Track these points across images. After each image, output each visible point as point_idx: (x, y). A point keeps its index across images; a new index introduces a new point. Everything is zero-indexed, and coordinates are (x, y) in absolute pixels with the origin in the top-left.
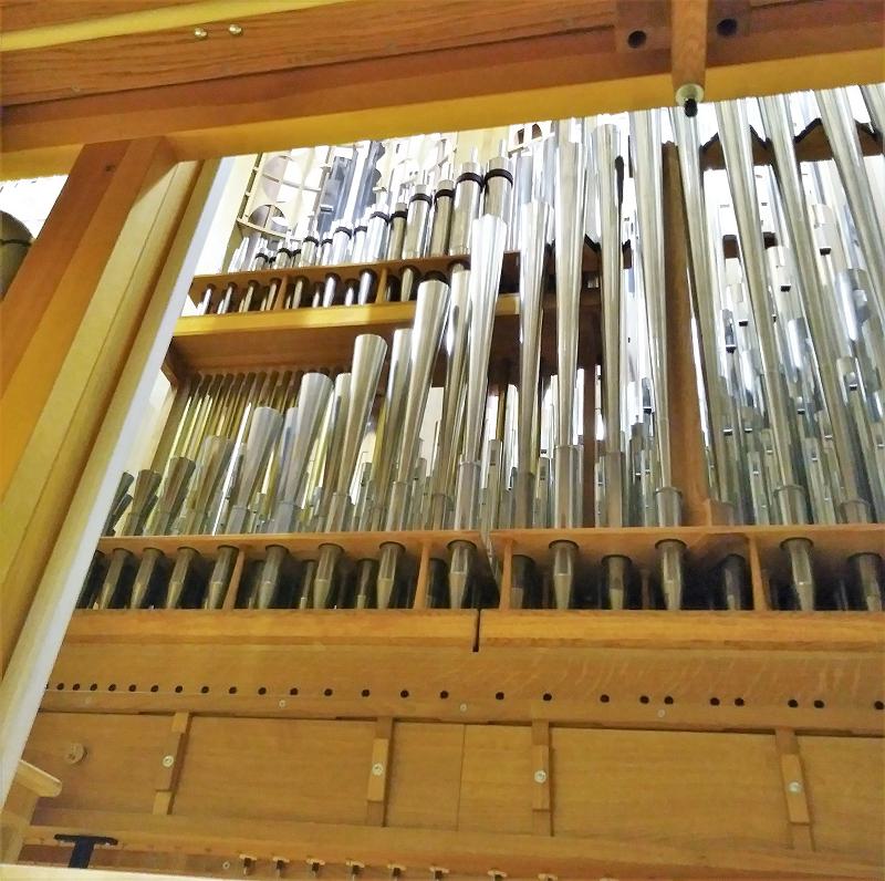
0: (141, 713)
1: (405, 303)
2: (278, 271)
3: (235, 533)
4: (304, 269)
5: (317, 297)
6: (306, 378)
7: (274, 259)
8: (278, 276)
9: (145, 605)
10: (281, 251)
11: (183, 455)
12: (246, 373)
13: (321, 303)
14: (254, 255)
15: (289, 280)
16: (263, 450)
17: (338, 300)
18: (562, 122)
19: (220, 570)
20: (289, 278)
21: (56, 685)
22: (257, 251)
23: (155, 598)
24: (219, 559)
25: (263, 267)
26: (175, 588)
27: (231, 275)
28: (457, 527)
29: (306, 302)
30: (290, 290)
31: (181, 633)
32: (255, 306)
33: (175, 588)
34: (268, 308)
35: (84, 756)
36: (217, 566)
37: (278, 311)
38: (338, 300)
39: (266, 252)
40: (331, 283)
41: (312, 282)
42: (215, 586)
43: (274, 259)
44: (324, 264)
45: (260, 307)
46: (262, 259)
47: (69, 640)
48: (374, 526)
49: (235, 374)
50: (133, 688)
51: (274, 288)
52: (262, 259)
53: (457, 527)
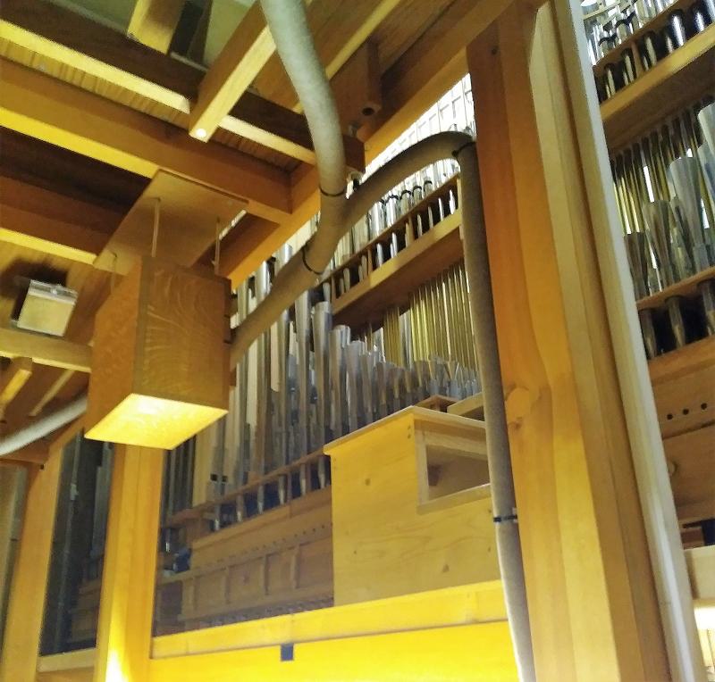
0: (704, 426)
1: (673, 53)
2: (625, 43)
3: (705, 268)
4: (646, 27)
5: (669, 42)
6: (701, 116)
7: (615, 35)
8: (627, 47)
9: (266, 508)
10: (617, 25)
11: (629, 232)
12: (648, 134)
13: (676, 45)
14: (596, 44)
15: (637, 44)
16: (693, 190)
17: (691, 31)
18: (316, 230)
19: (303, 474)
20: (636, 42)
21: (666, 416)
22: (597, 39)
23: (296, 493)
24: (704, 294)
25: (610, 49)
26: (678, 331)
27: (642, 30)
28: (661, 289)
29: (662, 53)
30: (643, 51)
31: (703, 359)
32: (620, 85)
33: (678, 331)
34: (632, 78)
35: (676, 470)
36: (705, 300)
37: (641, 76)
38: (691, 31)
39: (605, 34)
40: (676, 22)
41: (657, 32)
42: (303, 483)
43: (615, 35)
44: (661, 9)
45: (623, 81)
46: (605, 43)
47: (655, 383)
48: (241, 483)
49: (622, 153)
50: (686, 412)
51: (628, 58)
52: (605, 43)
53: (661, 289)
